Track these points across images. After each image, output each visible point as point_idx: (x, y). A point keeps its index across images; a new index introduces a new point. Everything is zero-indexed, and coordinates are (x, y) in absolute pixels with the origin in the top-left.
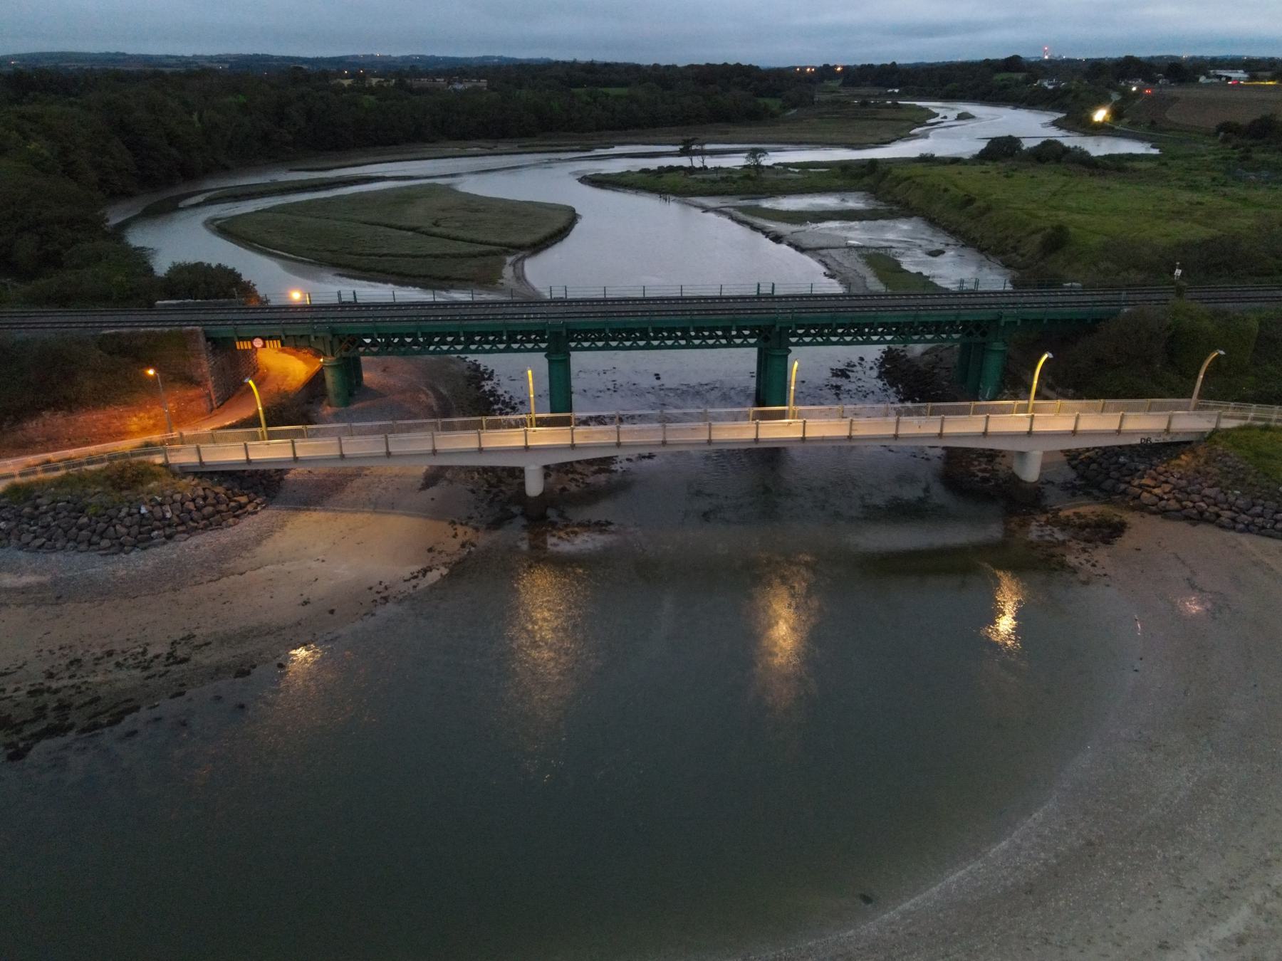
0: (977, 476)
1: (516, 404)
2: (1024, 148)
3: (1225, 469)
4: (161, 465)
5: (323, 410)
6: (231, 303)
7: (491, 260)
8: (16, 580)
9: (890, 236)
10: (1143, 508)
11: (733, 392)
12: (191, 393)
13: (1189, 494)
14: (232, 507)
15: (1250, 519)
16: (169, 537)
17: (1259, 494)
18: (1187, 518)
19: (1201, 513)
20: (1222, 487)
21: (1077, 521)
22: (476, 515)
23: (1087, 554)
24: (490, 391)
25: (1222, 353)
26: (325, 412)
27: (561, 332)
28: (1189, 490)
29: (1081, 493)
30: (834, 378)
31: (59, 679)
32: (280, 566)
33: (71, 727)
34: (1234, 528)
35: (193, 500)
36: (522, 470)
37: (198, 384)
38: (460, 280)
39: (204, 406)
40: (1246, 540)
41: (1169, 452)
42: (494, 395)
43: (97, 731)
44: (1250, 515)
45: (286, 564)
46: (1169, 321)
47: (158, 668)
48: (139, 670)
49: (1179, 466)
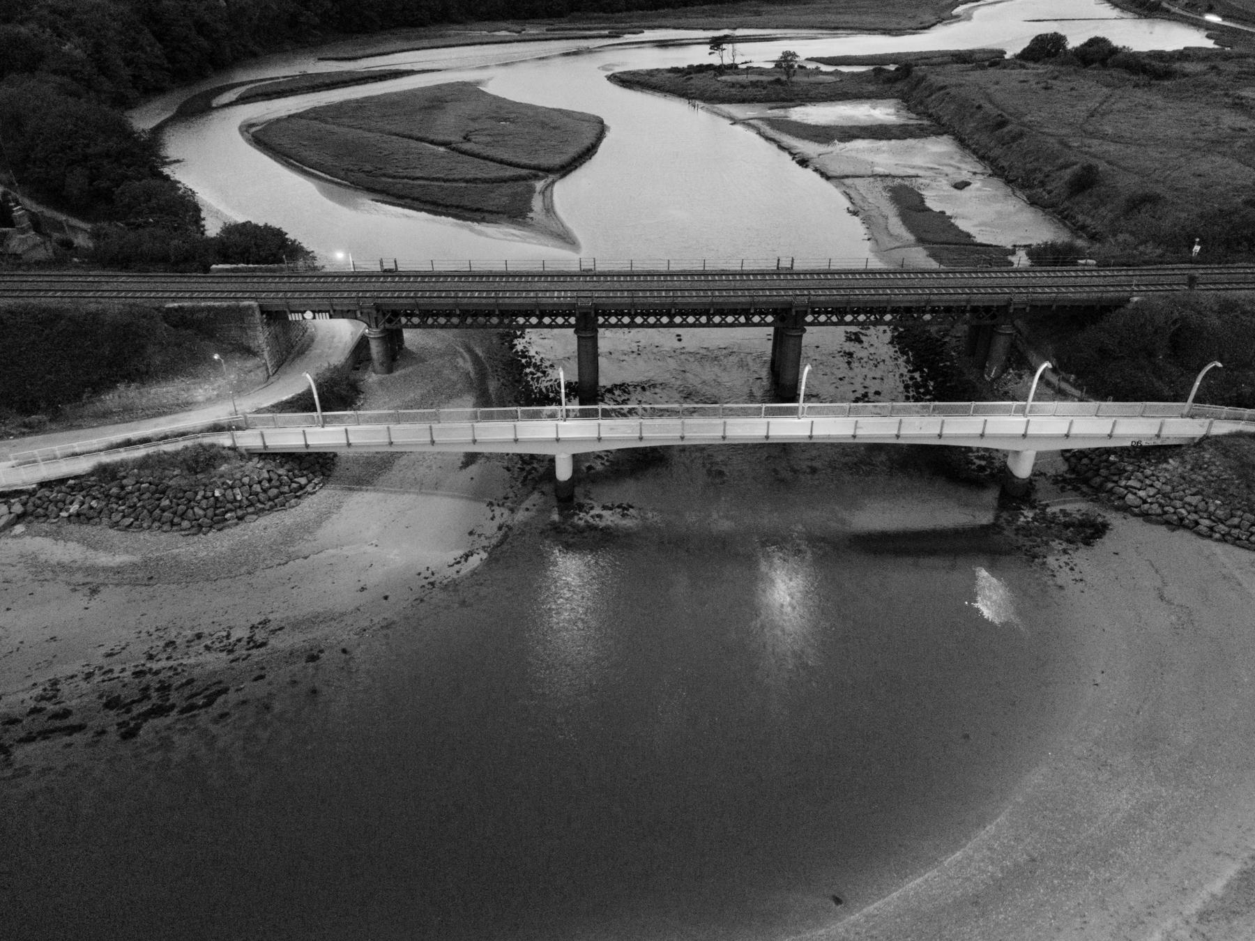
0: (974, 464)
1: (546, 367)
2: (1069, 47)
4: (230, 448)
6: (282, 270)
7: (520, 187)
8: (110, 559)
10: (1126, 509)
11: (749, 357)
12: (250, 364)
14: (294, 488)
15: (1227, 529)
16: (240, 518)
17: (1239, 506)
18: (1168, 523)
19: (1181, 519)
21: (1062, 519)
22: (511, 495)
23: (1067, 556)
24: (522, 351)
25: (1220, 365)
26: (370, 380)
27: (590, 313)
28: (1172, 496)
29: (1070, 487)
30: (848, 343)
31: (158, 661)
33: (173, 706)
34: (1210, 537)
35: (260, 482)
37: (255, 354)
38: (491, 212)
39: (261, 374)
40: (1219, 549)
42: (526, 357)
43: (194, 712)
44: (1229, 526)
46: (1176, 315)
47: (241, 651)
48: (225, 653)
49: (1166, 470)
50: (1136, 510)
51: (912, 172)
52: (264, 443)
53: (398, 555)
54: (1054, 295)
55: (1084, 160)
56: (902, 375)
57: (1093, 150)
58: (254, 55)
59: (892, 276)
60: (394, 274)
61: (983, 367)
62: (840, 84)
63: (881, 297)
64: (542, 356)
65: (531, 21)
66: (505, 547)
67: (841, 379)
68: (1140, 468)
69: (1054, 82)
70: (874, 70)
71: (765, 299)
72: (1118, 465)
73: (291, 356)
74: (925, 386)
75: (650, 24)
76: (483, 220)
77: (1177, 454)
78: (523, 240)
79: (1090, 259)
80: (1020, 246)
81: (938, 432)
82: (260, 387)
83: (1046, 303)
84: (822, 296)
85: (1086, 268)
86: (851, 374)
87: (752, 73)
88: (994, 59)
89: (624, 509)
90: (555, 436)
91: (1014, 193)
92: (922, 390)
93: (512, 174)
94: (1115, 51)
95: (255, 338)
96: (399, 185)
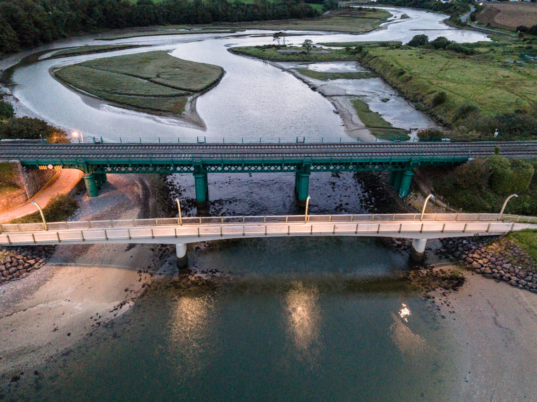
0: (396, 243)
1: (181, 191)
2: (429, 41)
3: (515, 254)
5: (84, 199)
7: (179, 99)
9: (365, 89)
10: (473, 270)
11: (284, 185)
12: (15, 193)
13: (496, 265)
14: (26, 266)
15: (525, 282)
17: (530, 270)
18: (494, 278)
19: (502, 276)
20: (512, 264)
21: (442, 275)
24: (170, 182)
25: (516, 196)
28: (496, 263)
30: (333, 178)
32: (46, 304)
34: (517, 286)
36: (175, 245)
37: (19, 188)
38: (164, 111)
39: (22, 199)
40: (523, 294)
41: (487, 240)
44: (526, 281)
45: (50, 303)
49: (492, 249)
50: (479, 270)
51: (363, 94)
52: (9, 241)
53: (80, 306)
54: (432, 156)
55: (440, 90)
56: (359, 194)
57: (443, 85)
58: (64, 37)
59: (353, 146)
60: (100, 145)
61: (398, 192)
62: (331, 55)
63: (346, 157)
64: (180, 184)
65: (195, 25)
66: (145, 297)
67: (329, 197)
68: (479, 248)
69: (424, 55)
70: (346, 48)
71: (289, 158)
72: (468, 245)
73: (44, 187)
74: (370, 200)
75: (249, 27)
76: (160, 115)
77: (497, 240)
78: (179, 124)
79: (448, 138)
80: (413, 129)
81: (377, 230)
82: (22, 205)
83: (429, 161)
84: (319, 157)
85: (445, 142)
86: (333, 194)
87: (293, 49)
88: (398, 46)
89: (214, 273)
90: (174, 235)
91: (409, 104)
92: (369, 203)
93: (177, 93)
94: (449, 43)
95: (19, 179)
96: (121, 98)
